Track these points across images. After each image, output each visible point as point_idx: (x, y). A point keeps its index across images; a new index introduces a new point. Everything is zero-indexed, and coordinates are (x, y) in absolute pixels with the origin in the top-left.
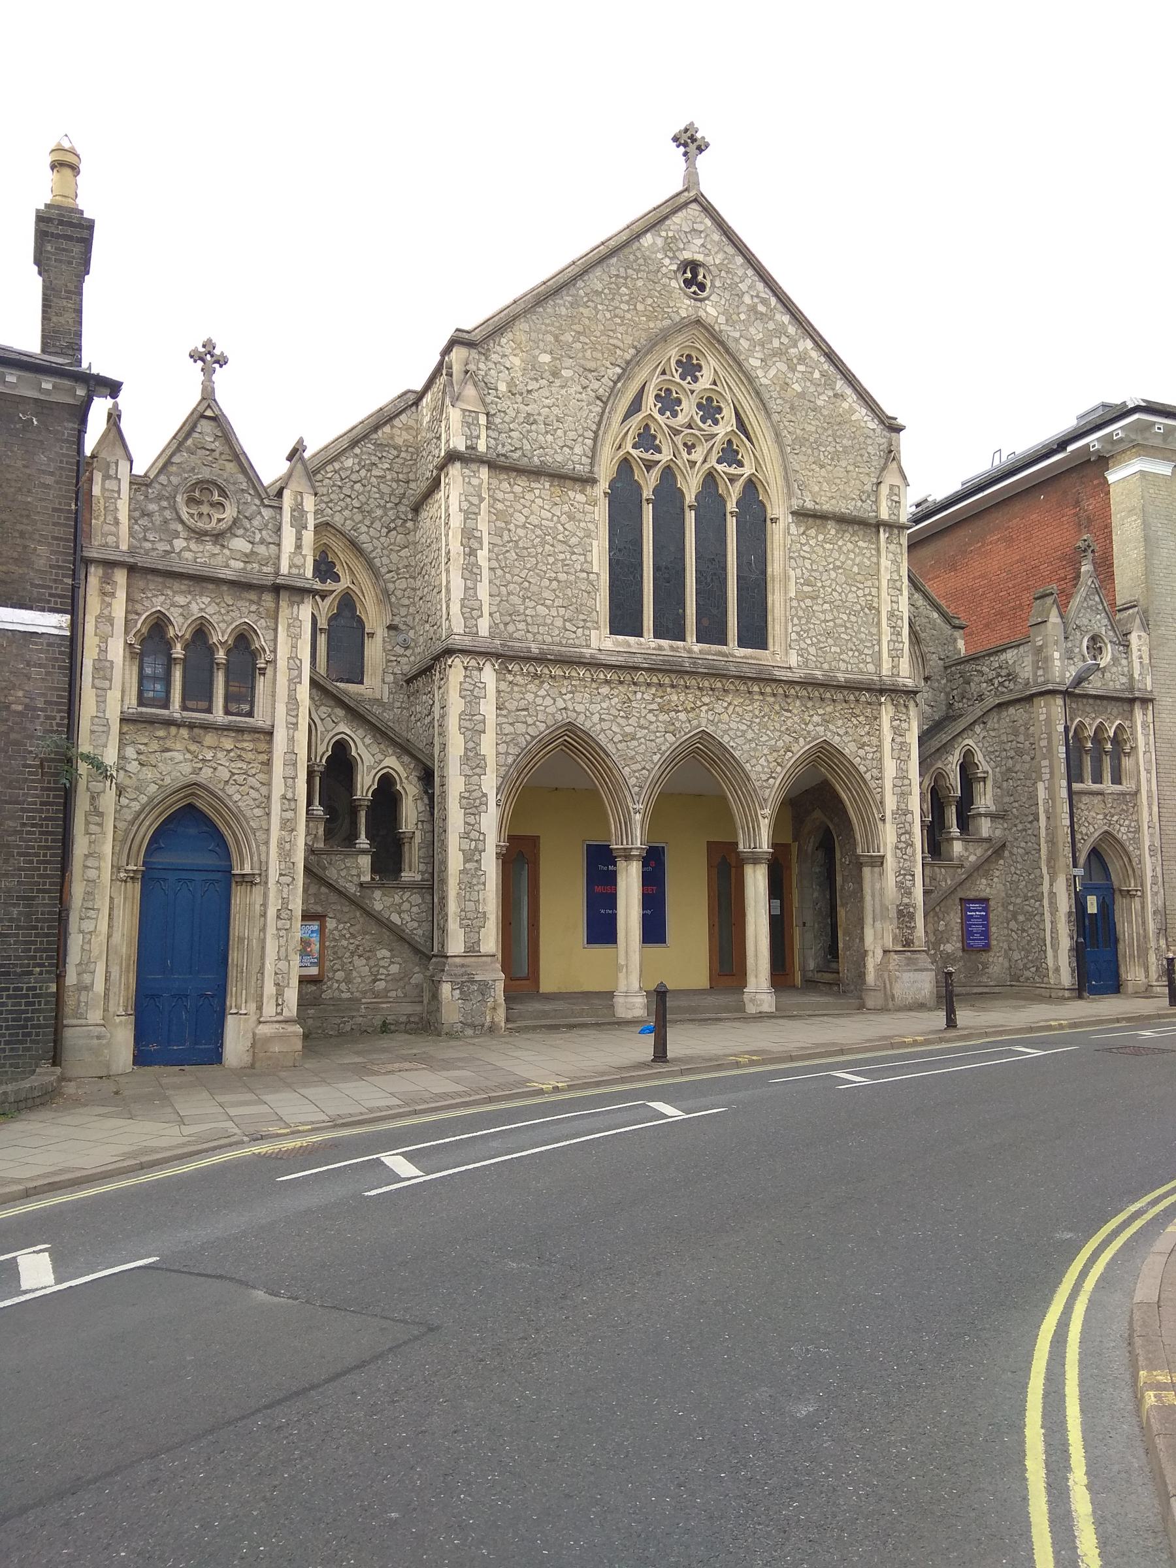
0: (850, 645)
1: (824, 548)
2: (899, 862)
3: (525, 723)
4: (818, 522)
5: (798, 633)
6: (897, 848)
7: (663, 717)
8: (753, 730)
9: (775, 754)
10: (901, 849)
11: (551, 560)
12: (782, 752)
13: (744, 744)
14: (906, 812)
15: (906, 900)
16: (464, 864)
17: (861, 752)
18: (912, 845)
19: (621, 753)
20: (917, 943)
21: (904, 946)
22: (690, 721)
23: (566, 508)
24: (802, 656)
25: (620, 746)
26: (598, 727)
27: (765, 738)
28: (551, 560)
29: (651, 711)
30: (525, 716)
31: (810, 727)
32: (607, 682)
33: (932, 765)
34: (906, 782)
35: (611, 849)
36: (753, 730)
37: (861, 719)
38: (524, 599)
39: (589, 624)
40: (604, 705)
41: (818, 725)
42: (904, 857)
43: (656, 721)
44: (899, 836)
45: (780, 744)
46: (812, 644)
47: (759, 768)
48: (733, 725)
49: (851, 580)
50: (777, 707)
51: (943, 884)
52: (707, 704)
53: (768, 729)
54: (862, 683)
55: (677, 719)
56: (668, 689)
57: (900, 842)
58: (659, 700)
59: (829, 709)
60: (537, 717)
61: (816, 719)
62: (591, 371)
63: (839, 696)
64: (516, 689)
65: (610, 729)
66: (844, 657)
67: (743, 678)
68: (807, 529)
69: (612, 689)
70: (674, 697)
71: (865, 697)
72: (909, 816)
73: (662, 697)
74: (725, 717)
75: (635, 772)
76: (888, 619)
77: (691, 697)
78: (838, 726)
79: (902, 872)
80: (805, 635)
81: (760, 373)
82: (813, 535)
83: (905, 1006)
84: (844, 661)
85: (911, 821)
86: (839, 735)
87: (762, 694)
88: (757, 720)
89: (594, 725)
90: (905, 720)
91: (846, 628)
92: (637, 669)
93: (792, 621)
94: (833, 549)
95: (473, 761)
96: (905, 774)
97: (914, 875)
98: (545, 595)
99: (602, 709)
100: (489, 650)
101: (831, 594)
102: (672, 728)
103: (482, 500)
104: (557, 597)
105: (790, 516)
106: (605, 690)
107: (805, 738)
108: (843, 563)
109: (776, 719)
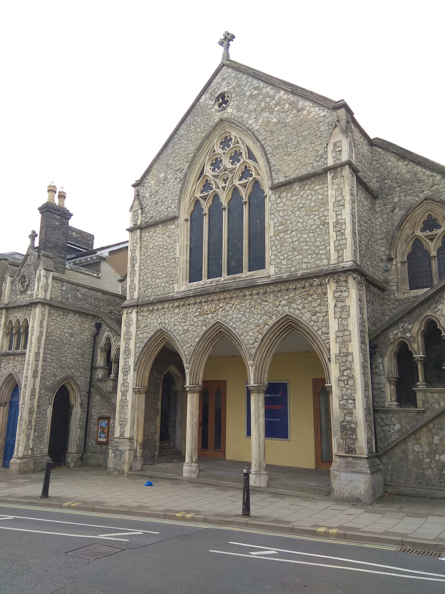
0: (309, 252)
1: (292, 201)
2: (342, 391)
3: (147, 332)
4: (287, 187)
5: (275, 255)
6: (340, 380)
7: (201, 318)
8: (246, 317)
9: (258, 328)
10: (343, 381)
11: (162, 258)
12: (262, 326)
13: (240, 325)
14: (347, 354)
15: (348, 418)
16: (122, 397)
17: (314, 318)
18: (352, 377)
19: (182, 340)
20: (358, 451)
21: (347, 452)
22: (213, 318)
23: (167, 234)
24: (278, 267)
25: (182, 336)
26: (173, 329)
27: (252, 319)
28: (162, 258)
29: (195, 316)
30: (147, 329)
31: (280, 308)
32: (178, 307)
33: (421, 315)
34: (347, 333)
35: (326, 387)
36: (246, 317)
37: (315, 296)
38: (152, 279)
39: (174, 282)
40: (176, 318)
41: (284, 306)
42: (347, 386)
43: (197, 321)
44: (342, 372)
45: (261, 321)
46: (284, 258)
47: (248, 337)
48: (235, 316)
49: (310, 212)
50: (259, 301)
51: (437, 406)
52: (222, 307)
53: (254, 314)
54: (312, 273)
55: (207, 318)
56: (203, 304)
57: (343, 375)
58: (199, 310)
59: (291, 295)
60: (150, 329)
61: (283, 302)
62: (178, 170)
63: (299, 285)
64: (144, 318)
65: (178, 329)
66: (305, 260)
67: (241, 289)
68: (281, 194)
69: (180, 309)
70: (206, 307)
71: (317, 281)
72: (350, 357)
73: (201, 308)
74: (231, 312)
75: (187, 348)
76: (334, 227)
77: (214, 306)
78: (298, 304)
79: (345, 397)
80: (280, 255)
81: (254, 125)
82: (285, 196)
83: (343, 498)
84: (305, 262)
85: (351, 360)
86: (298, 309)
87: (251, 295)
88: (248, 310)
89: (172, 328)
90: (345, 291)
91: (307, 242)
92: (189, 297)
93: (271, 249)
94: (297, 198)
95: (127, 352)
96: (346, 328)
97: (354, 400)
98: (159, 274)
99: (175, 320)
100: (133, 304)
101: (296, 225)
102: (205, 323)
103: (137, 243)
104: (163, 273)
105: (271, 191)
106: (177, 311)
107: (276, 315)
108: (304, 204)
109: (259, 307)
